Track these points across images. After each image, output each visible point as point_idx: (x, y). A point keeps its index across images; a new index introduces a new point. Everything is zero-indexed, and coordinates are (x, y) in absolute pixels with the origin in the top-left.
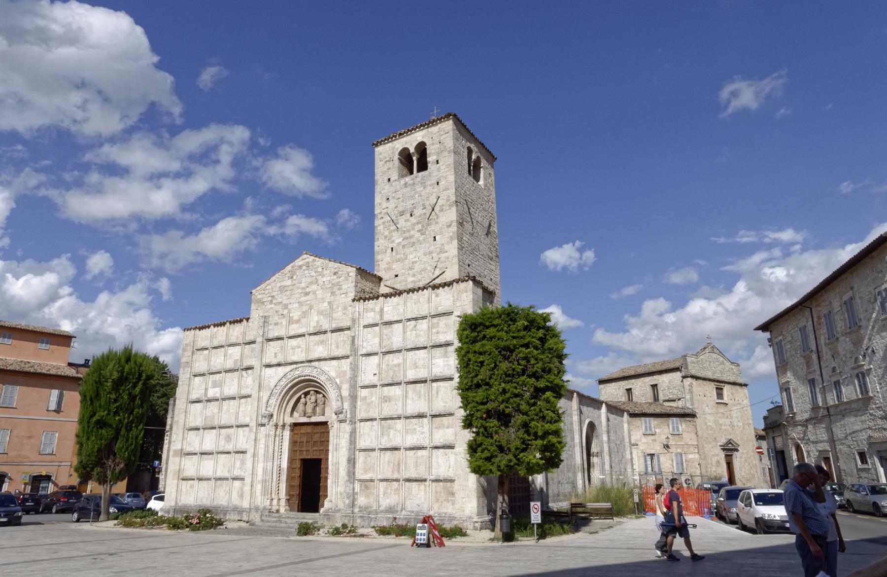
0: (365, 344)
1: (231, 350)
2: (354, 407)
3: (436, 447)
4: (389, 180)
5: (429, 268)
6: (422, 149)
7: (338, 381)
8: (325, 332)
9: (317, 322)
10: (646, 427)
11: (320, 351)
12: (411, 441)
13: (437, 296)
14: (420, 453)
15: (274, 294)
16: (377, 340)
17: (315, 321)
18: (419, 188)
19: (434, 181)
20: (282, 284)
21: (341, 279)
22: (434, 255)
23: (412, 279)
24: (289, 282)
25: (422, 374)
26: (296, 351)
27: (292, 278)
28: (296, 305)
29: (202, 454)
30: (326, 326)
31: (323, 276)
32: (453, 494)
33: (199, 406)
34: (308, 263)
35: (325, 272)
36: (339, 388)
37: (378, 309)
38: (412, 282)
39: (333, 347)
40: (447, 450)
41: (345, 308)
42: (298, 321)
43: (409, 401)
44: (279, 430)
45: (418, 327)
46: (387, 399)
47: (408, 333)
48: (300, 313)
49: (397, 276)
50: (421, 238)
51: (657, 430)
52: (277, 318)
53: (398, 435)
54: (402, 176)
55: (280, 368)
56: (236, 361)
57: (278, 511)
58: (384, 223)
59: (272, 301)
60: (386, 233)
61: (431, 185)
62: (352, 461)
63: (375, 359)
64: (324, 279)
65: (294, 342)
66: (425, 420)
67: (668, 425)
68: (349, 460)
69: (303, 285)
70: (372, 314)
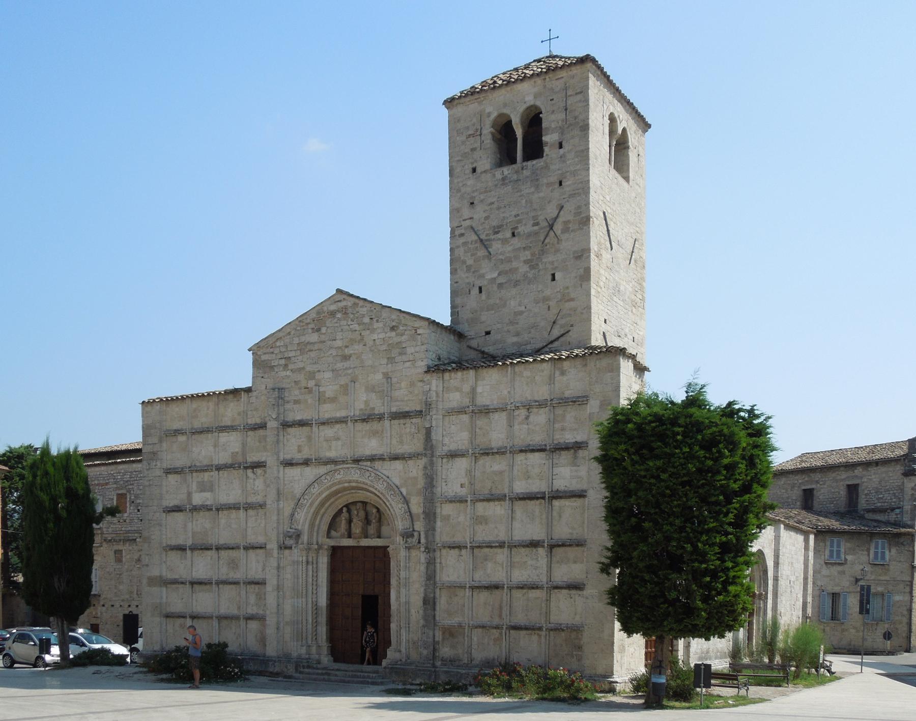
0: (446, 441)
1: (224, 437)
2: (431, 529)
3: (556, 587)
4: (474, 170)
5: (543, 324)
6: (534, 121)
7: (404, 491)
8: (381, 417)
9: (366, 402)
10: (831, 552)
11: (372, 446)
12: (519, 576)
13: (563, 373)
14: (533, 594)
15: (291, 354)
16: (465, 435)
17: (361, 400)
18: (527, 189)
19: (554, 179)
20: (303, 339)
21: (404, 338)
22: (552, 303)
23: (515, 339)
24: (314, 337)
25: (537, 486)
26: (334, 443)
27: (319, 330)
28: (328, 375)
29: (192, 583)
30: (379, 408)
31: (373, 331)
32: (580, 648)
33: (179, 516)
34: (346, 308)
35: (376, 325)
36: (406, 502)
37: (466, 388)
38: (514, 344)
39: (394, 442)
40: (573, 592)
41: (412, 384)
42: (333, 400)
43: (516, 525)
44: (312, 555)
45: (531, 419)
46: (480, 520)
47: (516, 427)
48: (336, 387)
49: (488, 333)
50: (530, 275)
51: (849, 558)
52: (297, 392)
53: (495, 569)
54: (500, 164)
55: (308, 470)
56: (234, 455)
57: (319, 662)
58: (465, 244)
59: (286, 365)
60: (470, 262)
61: (549, 185)
62: (429, 603)
63: (462, 464)
64: (375, 336)
65: (328, 432)
66: (540, 550)
67: (868, 550)
68: (426, 601)
69: (339, 343)
70: (458, 394)
